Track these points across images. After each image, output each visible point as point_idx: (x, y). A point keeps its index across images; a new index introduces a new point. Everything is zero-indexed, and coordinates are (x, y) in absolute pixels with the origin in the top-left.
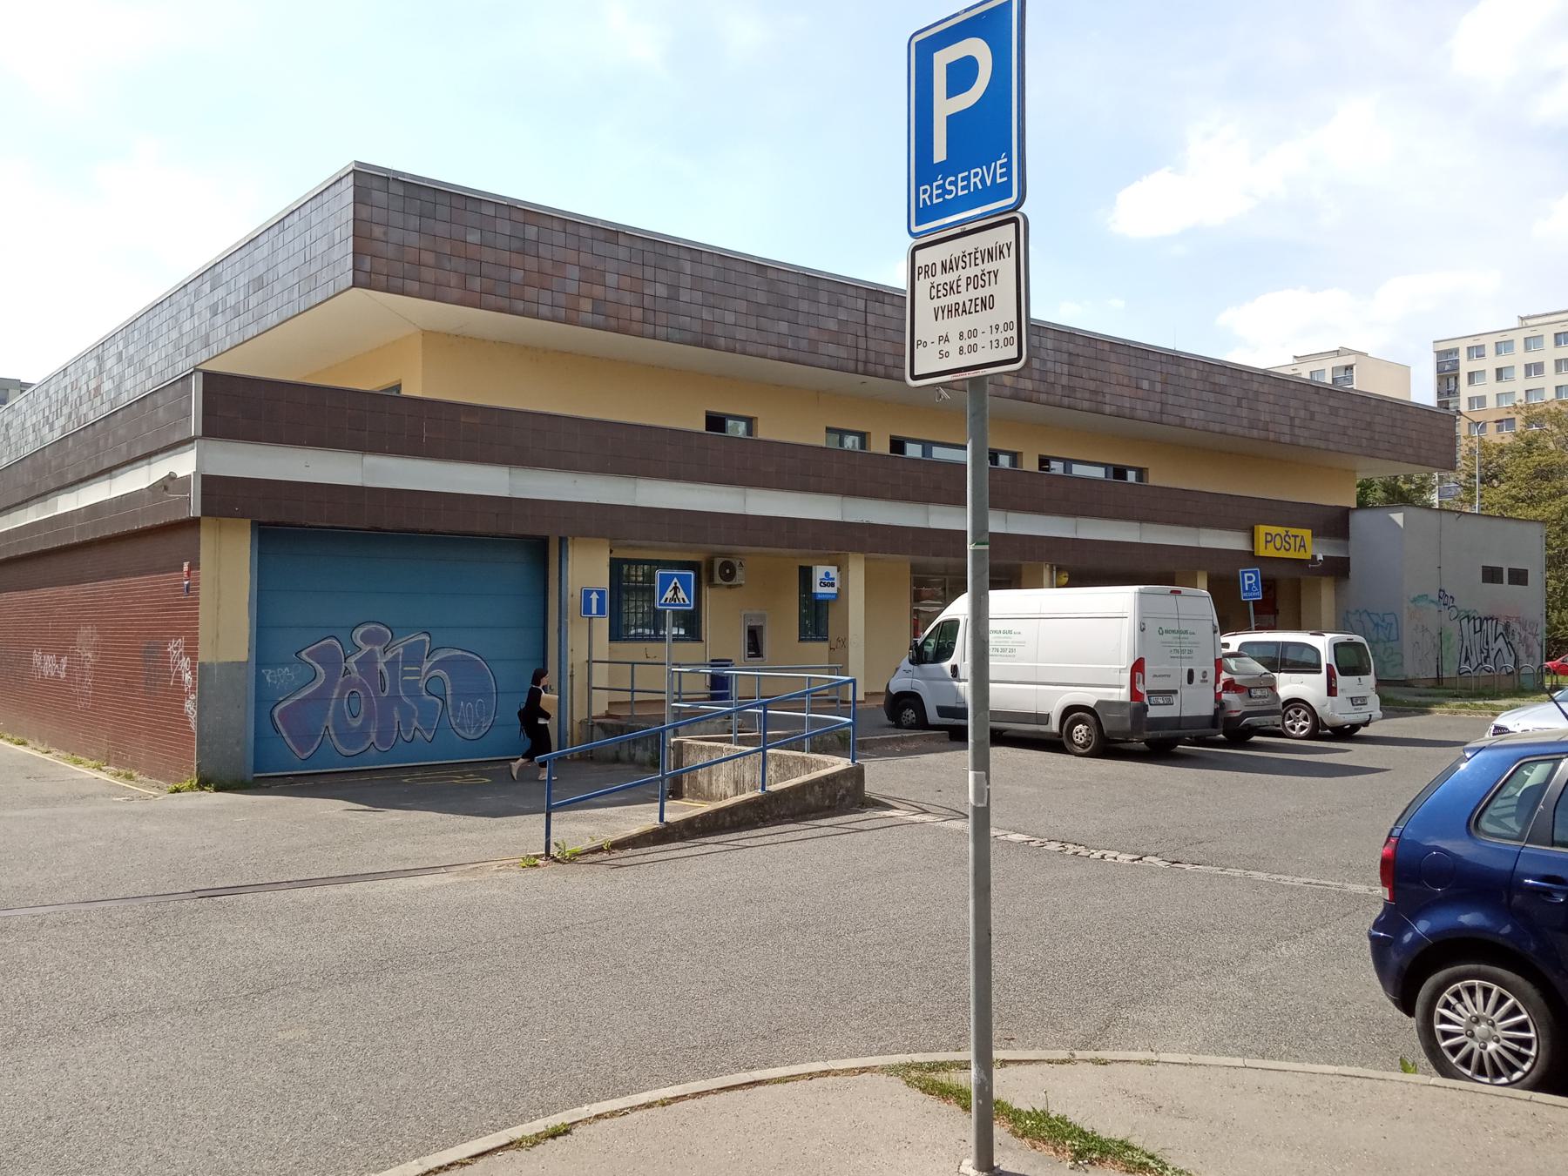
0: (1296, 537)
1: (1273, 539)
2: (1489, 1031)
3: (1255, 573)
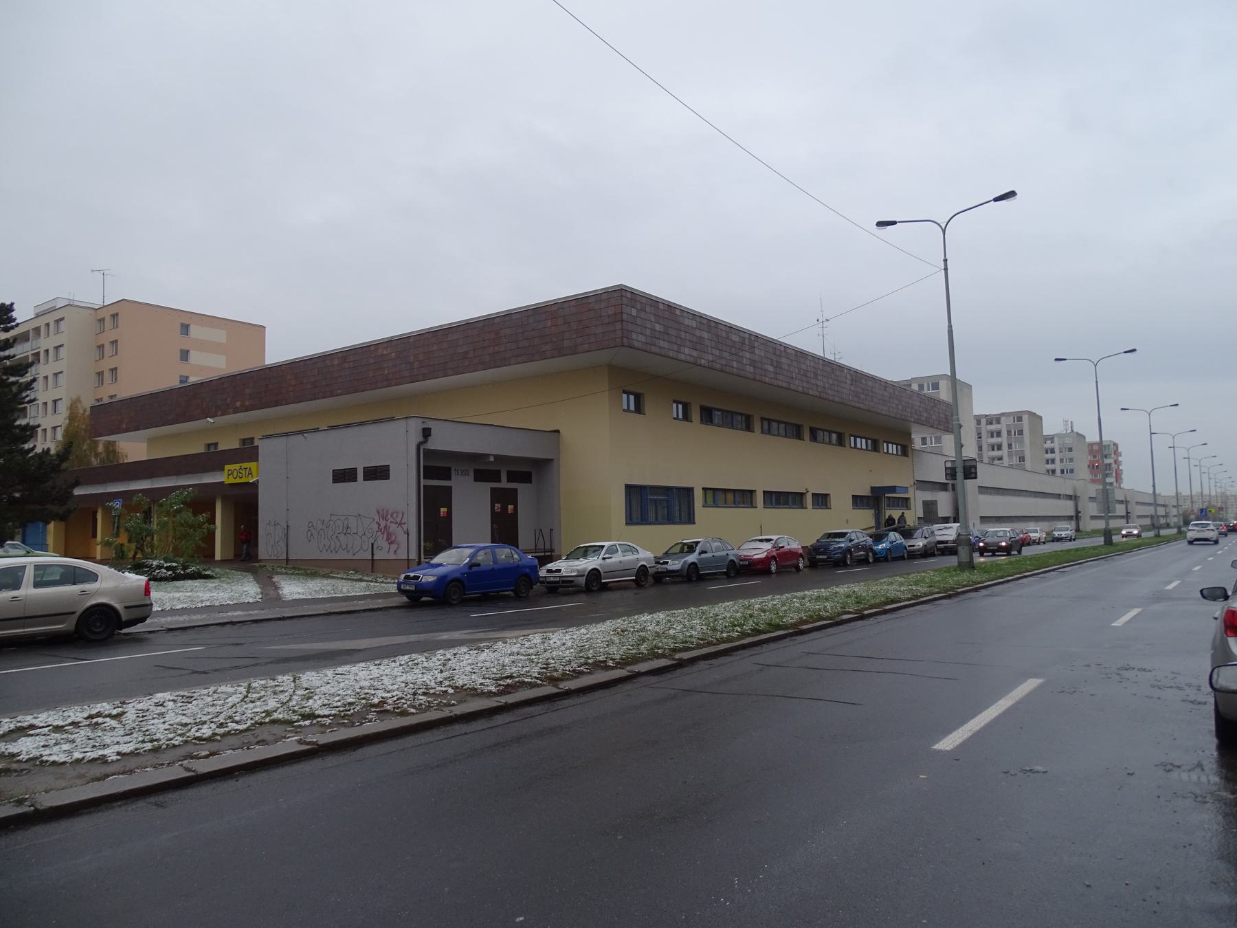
1: (232, 473)
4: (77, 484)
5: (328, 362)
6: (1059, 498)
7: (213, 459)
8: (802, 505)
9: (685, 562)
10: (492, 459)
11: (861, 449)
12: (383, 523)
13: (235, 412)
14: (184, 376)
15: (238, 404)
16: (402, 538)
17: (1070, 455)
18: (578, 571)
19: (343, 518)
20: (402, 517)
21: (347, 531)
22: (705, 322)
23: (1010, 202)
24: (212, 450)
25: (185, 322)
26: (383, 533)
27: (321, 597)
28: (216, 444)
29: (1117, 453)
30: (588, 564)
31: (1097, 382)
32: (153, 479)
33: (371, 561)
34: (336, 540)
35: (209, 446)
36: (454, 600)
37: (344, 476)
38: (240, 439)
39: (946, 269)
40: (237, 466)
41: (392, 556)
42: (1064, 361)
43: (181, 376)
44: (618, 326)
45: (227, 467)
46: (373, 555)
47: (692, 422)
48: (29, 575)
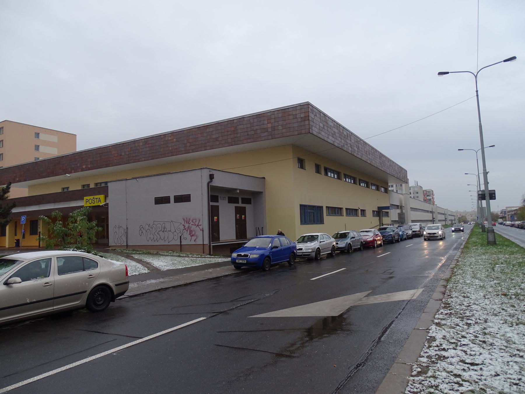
0: (97, 198)
1: (89, 201)
2: (460, 393)
3: (25, 217)
4: (14, 206)
5: (137, 145)
6: (428, 212)
7: (86, 191)
8: (357, 215)
9: (347, 243)
10: (238, 191)
11: (373, 189)
12: (187, 225)
13: (82, 171)
14: (37, 158)
15: (84, 167)
16: (199, 233)
17: (417, 195)
18: (312, 249)
19: (161, 223)
20: (199, 222)
21: (164, 230)
22: (336, 124)
23: (512, 62)
24: (65, 190)
25: (37, 132)
26: (187, 231)
27: (181, 268)
28: (68, 188)
29: (433, 194)
30: (316, 245)
31: (477, 160)
32: (40, 205)
33: (180, 246)
34: (157, 235)
35: (63, 189)
36: (266, 268)
37: (161, 201)
38: (82, 185)
39: (477, 96)
40: (92, 197)
41: (193, 243)
42: (490, 146)
43: (35, 158)
44: (307, 122)
45: (85, 198)
46: (181, 242)
47: (321, 174)
48: (54, 265)
